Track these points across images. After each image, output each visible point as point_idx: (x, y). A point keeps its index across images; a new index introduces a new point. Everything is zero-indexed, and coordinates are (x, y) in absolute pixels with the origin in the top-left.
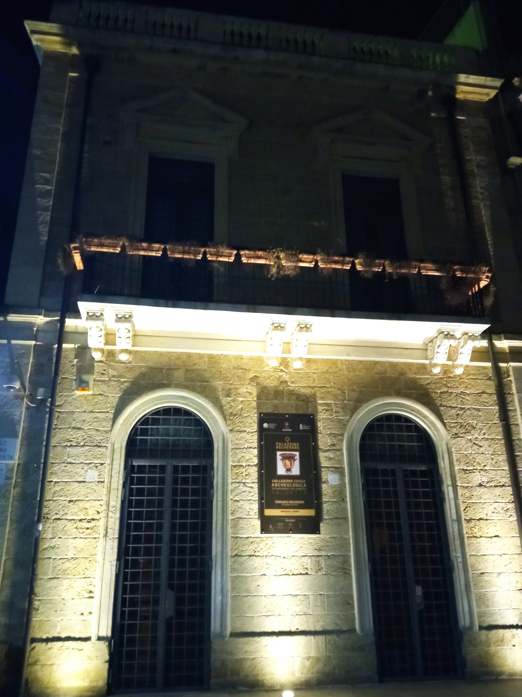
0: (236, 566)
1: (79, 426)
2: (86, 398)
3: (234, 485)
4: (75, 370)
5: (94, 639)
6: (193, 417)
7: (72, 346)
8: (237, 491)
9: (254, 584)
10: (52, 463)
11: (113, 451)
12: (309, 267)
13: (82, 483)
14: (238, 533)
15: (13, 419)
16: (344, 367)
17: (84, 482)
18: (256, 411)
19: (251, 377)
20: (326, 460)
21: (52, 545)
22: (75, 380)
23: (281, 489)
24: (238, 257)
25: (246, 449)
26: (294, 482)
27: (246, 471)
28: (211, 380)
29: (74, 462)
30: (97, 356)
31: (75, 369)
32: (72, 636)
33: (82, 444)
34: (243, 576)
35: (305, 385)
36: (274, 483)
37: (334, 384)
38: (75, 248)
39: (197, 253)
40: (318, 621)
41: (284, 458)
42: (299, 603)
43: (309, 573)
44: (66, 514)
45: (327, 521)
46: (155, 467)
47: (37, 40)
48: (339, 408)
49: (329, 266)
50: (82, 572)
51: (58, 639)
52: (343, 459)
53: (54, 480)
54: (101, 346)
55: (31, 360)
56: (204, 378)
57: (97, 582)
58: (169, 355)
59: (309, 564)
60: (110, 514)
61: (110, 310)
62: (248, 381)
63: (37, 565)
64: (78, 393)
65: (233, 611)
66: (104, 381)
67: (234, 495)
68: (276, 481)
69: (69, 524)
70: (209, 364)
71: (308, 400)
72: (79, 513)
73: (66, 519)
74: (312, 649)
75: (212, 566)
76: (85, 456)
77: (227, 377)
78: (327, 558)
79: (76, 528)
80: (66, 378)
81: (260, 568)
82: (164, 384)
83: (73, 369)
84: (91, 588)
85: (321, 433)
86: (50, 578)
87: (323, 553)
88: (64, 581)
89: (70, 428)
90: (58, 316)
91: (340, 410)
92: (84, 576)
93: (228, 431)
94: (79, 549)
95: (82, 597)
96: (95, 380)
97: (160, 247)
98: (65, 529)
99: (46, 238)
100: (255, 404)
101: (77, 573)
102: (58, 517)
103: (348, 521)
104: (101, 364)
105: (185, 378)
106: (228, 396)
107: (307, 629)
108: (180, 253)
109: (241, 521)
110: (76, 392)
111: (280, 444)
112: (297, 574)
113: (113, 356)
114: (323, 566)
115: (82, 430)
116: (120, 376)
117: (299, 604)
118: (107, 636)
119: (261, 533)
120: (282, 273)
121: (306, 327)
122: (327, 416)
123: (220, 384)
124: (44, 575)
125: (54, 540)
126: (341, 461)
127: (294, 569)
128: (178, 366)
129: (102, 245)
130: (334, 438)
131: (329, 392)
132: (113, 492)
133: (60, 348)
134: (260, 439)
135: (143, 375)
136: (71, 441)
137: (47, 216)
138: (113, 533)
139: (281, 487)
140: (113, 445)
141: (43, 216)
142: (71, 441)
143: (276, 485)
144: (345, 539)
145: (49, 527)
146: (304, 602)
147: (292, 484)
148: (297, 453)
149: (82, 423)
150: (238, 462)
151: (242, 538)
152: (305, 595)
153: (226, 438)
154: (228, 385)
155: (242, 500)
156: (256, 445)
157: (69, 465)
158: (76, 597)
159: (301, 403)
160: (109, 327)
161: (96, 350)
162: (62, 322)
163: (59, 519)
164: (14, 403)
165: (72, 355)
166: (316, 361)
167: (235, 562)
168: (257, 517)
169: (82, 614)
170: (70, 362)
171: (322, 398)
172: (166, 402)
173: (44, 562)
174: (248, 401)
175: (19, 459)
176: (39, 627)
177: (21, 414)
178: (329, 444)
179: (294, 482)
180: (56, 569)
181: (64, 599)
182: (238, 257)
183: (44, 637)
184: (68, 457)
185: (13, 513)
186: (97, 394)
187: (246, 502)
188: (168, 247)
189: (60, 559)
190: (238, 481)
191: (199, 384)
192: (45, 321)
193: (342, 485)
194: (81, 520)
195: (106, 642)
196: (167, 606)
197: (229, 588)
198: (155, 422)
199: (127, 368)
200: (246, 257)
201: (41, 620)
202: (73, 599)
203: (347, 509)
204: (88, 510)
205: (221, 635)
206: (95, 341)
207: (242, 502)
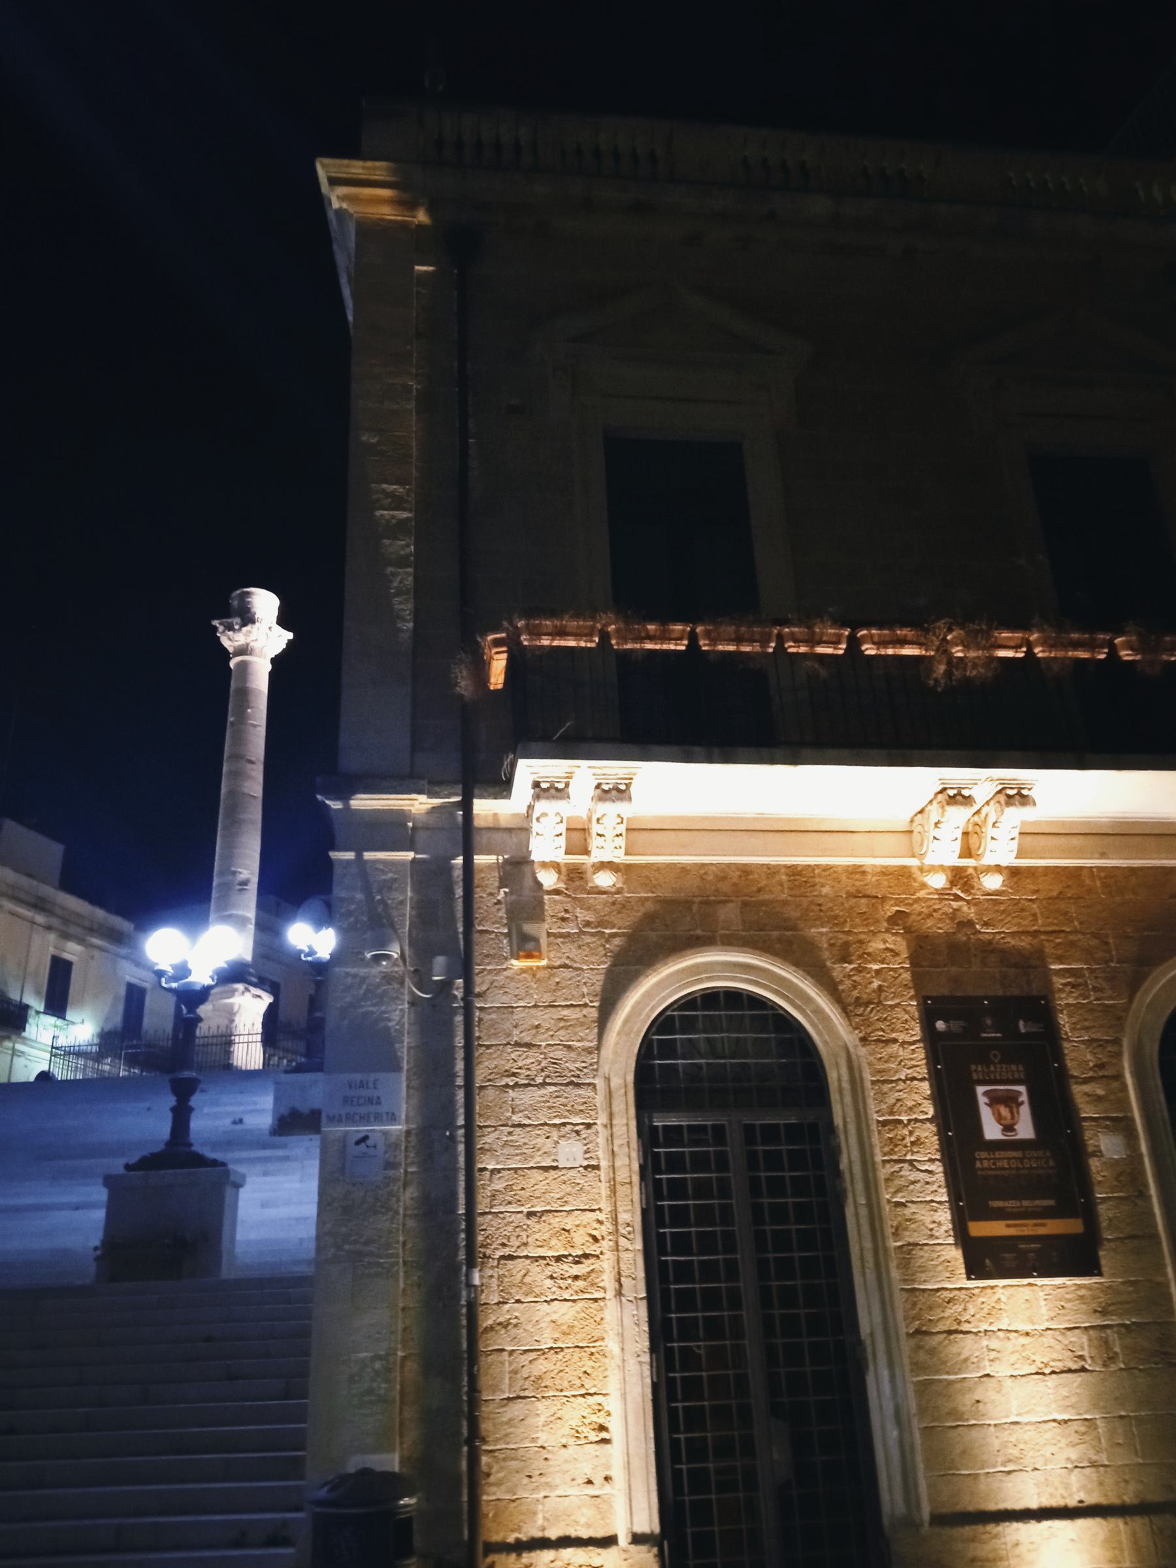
0: (922, 1356)
1: (527, 1040)
2: (534, 975)
3: (890, 1169)
4: (502, 913)
5: (623, 1540)
6: (770, 1012)
7: (491, 859)
8: (899, 1182)
9: (969, 1399)
10: (480, 1127)
11: (610, 1094)
12: (1013, 658)
13: (552, 1172)
14: (914, 1281)
15: (388, 1029)
16: (1098, 883)
17: (555, 1168)
18: (912, 992)
19: (889, 914)
20: (1088, 1102)
21: (501, 1319)
22: (508, 935)
23: (998, 1173)
24: (854, 644)
25: (904, 1081)
26: (1025, 1157)
27: (911, 1133)
28: (801, 925)
29: (527, 1122)
30: (549, 880)
31: (504, 910)
32: (573, 1534)
33: (539, 1080)
34: (940, 1381)
35: (1015, 929)
36: (981, 1160)
37: (1081, 923)
38: (497, 643)
39: (765, 643)
40: (1126, 1481)
41: (995, 1100)
42: (1075, 1438)
43: (1087, 1366)
44: (525, 1244)
45: (1113, 1245)
46: (703, 1128)
47: (341, 198)
48: (1100, 981)
49: (1061, 654)
50: (578, 1383)
51: (543, 1543)
52: (1128, 1098)
53: (490, 1167)
54: (561, 857)
55: (409, 894)
56: (786, 920)
57: (613, 1404)
58: (702, 872)
59: (1086, 1347)
60: (623, 1242)
61: (583, 774)
62: (886, 924)
63: (478, 1370)
64: (517, 964)
65: (929, 1466)
66: (568, 935)
67: (892, 1190)
68: (984, 1155)
69: (535, 1268)
70: (791, 889)
71: (1028, 963)
72: (554, 1242)
73: (527, 1257)
74: (1122, 1550)
75: (866, 1359)
76: (549, 1108)
77: (836, 917)
78: (1123, 1330)
79: (552, 1277)
80: (486, 932)
81: (975, 1360)
82: (698, 938)
83: (499, 910)
84: (601, 1419)
85: (1067, 1040)
86: (509, 1399)
87: (1114, 1320)
88: (538, 1404)
89: (509, 1044)
90: (456, 794)
91: (1104, 985)
92: (583, 1391)
93: (857, 1042)
94: (564, 1327)
95: (583, 1441)
96: (549, 934)
97: (684, 630)
98: (527, 1280)
99: (411, 625)
100: (907, 976)
101: (566, 1384)
102: (507, 1251)
103: (1159, 1243)
104: (557, 897)
105: (744, 922)
106: (845, 959)
107: (1103, 1501)
108: (729, 641)
109: (917, 1252)
110: (514, 962)
111: (980, 1068)
112: (1062, 1372)
113: (582, 878)
114: (1117, 1349)
115: (535, 1049)
116: (601, 924)
117: (1078, 1441)
118: (652, 1532)
119: (969, 1278)
120: (957, 674)
121: (1019, 794)
122: (1076, 998)
123: (822, 934)
124: (494, 1392)
125: (507, 1307)
126: (1124, 1103)
127: (1054, 1360)
128: (725, 894)
129: (562, 633)
130: (1099, 1050)
131: (1072, 944)
132: (622, 1191)
133: (468, 865)
134: (933, 1057)
135: (650, 919)
136: (514, 1074)
137: (404, 578)
138: (635, 1286)
139: (996, 1169)
140: (608, 1080)
141: (399, 579)
142: (514, 1074)
143: (986, 1164)
144: (1159, 1284)
145: (492, 1276)
146: (1086, 1438)
147: (1021, 1160)
148: (1022, 1089)
149: (534, 1031)
150: (891, 1113)
151: (924, 1290)
152: (1086, 1419)
153: (854, 1057)
154: (842, 936)
155: (913, 1202)
156: (923, 1071)
157: (518, 1130)
158: (571, 1441)
159: (1012, 971)
160: (590, 815)
161: (544, 865)
162: (466, 806)
163: (511, 1257)
164: (385, 993)
165: (493, 880)
166: (1031, 872)
167: (919, 1347)
168: (951, 1240)
169: (590, 1482)
170: (491, 894)
171: (1060, 959)
172: (709, 979)
173: (490, 1359)
174: (891, 969)
175: (407, 1121)
176: (495, 1516)
177: (399, 1015)
178: (1091, 1064)
179: (1025, 1157)
180: (518, 1376)
181: (543, 1448)
182: (854, 644)
183: (511, 1539)
184: (513, 1113)
185: (409, 1246)
186: (557, 964)
187: (922, 1206)
188: (699, 629)
189: (526, 1351)
190: (895, 1157)
191: (775, 934)
192: (429, 806)
193: (1134, 1158)
194: (558, 1259)
195: (653, 1546)
196: (774, 1456)
197: (913, 1408)
198: (688, 1025)
199: (614, 903)
200: (874, 643)
201: (498, 1500)
202: (565, 1446)
203: (1153, 1215)
204: (573, 1234)
205: (910, 1523)
206: (547, 846)
207: (913, 1208)
